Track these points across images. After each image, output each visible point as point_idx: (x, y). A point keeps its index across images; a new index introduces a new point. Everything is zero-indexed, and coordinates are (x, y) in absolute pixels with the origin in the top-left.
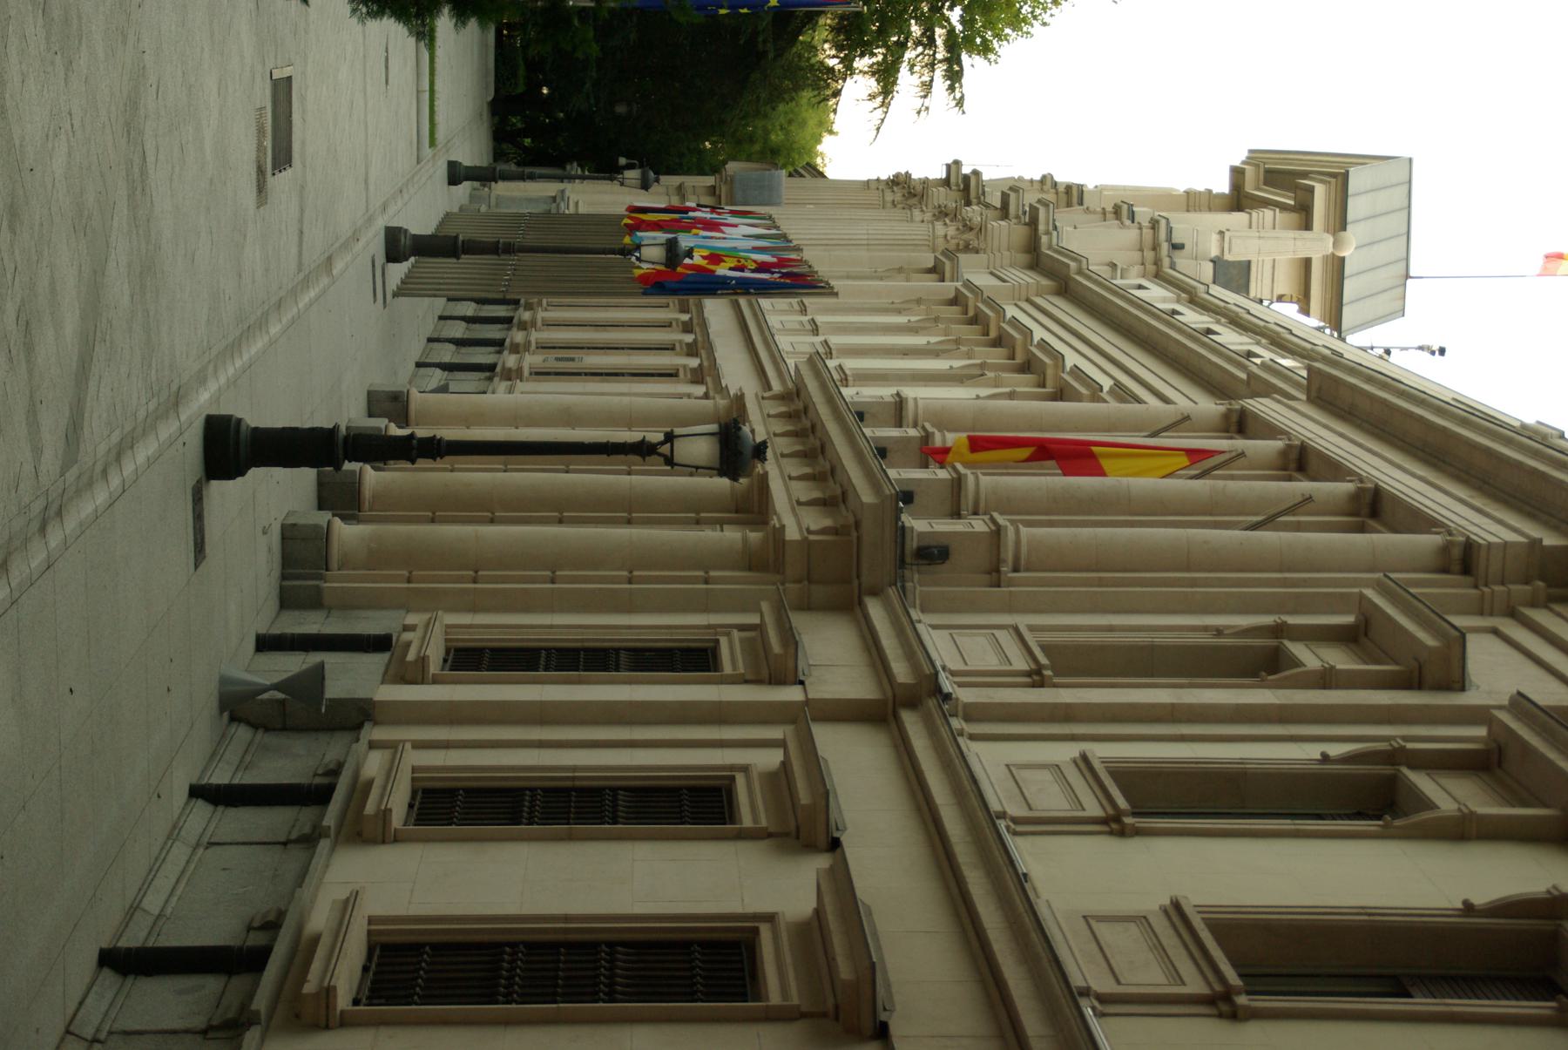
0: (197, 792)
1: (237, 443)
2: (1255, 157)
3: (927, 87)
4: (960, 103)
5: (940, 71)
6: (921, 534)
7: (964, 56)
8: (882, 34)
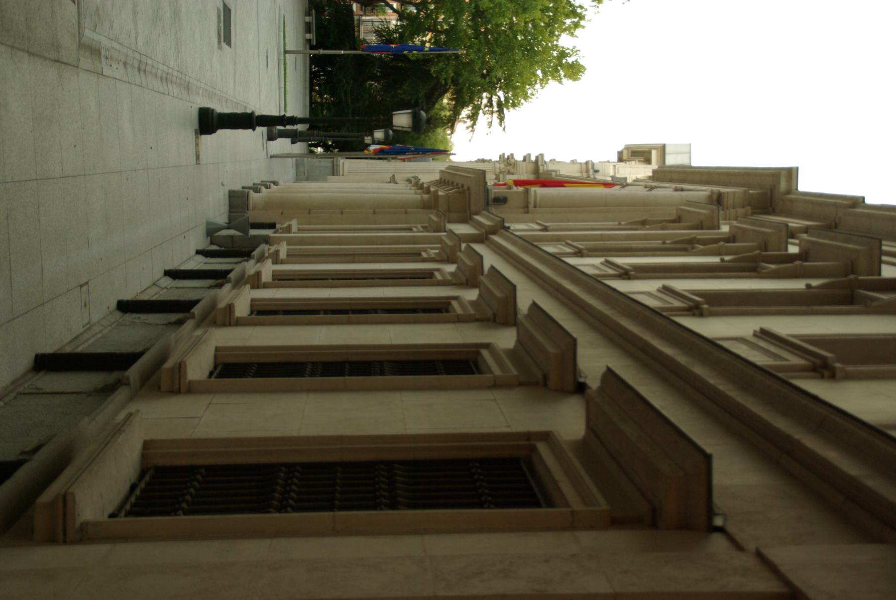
0: (198, 252)
1: (212, 117)
2: (627, 148)
3: (490, 124)
4: (504, 129)
5: (495, 115)
6: (495, 193)
7: (505, 109)
8: (471, 100)
